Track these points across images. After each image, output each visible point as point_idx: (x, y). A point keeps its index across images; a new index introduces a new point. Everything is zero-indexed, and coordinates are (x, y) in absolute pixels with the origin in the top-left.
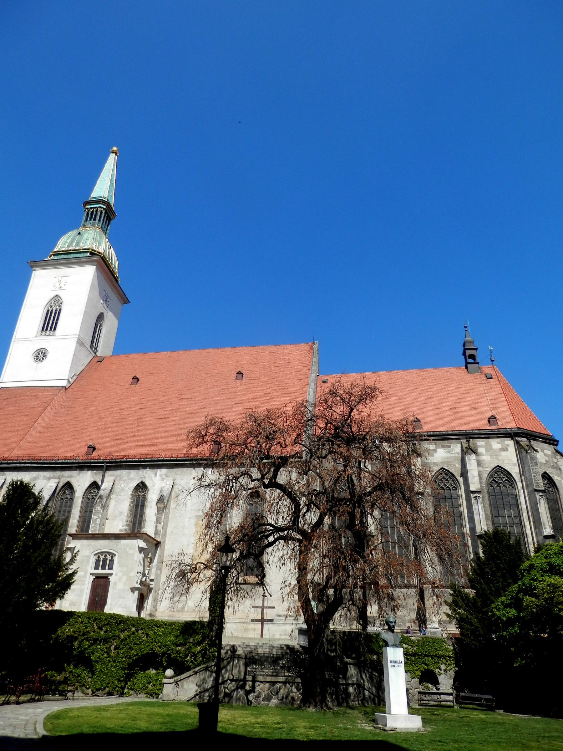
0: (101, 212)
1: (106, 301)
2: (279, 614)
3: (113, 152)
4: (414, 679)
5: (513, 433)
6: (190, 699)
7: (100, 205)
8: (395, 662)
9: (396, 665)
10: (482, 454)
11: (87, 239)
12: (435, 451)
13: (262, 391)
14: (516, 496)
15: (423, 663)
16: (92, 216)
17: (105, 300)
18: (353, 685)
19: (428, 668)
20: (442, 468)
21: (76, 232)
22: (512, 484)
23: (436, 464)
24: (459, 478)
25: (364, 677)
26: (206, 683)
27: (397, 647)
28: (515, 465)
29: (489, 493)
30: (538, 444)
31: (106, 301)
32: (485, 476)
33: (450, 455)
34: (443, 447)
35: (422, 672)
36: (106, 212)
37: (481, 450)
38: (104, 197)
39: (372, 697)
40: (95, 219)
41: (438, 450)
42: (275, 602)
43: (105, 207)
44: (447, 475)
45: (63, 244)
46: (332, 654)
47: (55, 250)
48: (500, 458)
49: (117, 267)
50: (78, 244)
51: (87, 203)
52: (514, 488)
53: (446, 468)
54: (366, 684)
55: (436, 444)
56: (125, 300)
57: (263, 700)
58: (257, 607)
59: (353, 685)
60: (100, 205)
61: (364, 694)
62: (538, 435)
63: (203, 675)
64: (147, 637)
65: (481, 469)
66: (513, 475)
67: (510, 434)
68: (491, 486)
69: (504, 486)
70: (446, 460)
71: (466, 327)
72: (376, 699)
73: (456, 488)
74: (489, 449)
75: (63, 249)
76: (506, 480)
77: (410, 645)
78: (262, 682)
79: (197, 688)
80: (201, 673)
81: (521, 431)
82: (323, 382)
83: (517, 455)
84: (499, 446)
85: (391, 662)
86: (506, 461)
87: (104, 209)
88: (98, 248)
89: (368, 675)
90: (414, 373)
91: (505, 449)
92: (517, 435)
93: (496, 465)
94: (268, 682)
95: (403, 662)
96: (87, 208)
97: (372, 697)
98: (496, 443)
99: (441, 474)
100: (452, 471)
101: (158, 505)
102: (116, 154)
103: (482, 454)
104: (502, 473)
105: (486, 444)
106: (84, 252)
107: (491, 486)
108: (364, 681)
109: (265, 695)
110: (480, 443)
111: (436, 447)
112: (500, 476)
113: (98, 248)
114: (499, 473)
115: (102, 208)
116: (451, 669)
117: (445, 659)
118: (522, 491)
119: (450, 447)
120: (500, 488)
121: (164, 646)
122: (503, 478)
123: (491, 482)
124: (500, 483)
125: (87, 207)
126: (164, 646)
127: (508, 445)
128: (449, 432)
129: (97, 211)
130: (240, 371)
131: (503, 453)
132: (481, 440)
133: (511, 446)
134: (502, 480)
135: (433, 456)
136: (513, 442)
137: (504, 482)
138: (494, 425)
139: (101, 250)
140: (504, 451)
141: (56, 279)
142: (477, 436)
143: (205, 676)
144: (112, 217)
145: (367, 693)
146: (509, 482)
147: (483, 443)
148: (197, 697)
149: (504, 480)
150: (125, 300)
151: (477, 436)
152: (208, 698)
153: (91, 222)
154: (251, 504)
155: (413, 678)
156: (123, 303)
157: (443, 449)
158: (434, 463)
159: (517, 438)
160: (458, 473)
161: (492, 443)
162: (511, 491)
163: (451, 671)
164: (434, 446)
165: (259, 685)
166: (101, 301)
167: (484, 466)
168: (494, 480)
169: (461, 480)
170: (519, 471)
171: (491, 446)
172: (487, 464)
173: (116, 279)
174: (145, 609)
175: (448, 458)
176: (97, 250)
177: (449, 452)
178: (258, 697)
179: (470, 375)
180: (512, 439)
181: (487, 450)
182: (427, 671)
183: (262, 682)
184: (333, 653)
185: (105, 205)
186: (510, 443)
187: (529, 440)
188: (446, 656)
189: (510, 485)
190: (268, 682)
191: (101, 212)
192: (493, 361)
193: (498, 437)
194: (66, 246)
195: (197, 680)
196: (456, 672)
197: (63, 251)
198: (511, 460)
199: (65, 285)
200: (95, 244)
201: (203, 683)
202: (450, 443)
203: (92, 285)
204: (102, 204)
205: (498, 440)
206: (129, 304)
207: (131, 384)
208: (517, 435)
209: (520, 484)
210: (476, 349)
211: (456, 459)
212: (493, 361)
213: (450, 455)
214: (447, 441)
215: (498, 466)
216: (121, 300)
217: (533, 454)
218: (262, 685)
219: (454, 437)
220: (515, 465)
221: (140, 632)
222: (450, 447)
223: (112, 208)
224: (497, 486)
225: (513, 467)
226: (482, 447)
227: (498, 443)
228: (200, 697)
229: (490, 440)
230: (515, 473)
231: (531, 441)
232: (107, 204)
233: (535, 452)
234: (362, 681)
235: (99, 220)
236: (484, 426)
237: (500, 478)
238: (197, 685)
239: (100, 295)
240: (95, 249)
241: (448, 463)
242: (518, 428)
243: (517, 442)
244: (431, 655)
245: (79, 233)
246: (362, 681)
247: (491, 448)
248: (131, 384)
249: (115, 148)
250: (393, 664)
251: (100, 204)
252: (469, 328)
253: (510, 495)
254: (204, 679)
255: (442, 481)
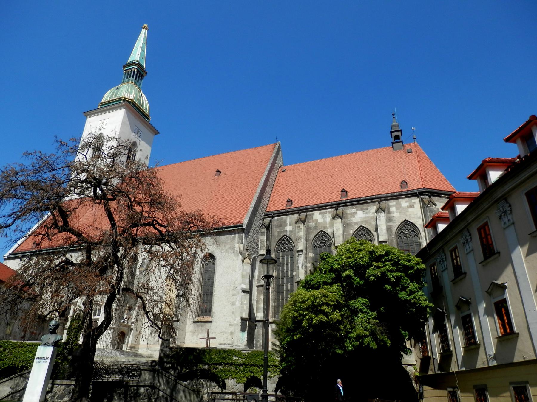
0: (134, 71)
1: (138, 133)
2: (221, 343)
3: (144, 28)
4: (240, 384)
5: (419, 193)
6: (2, 398)
7: (134, 67)
8: (41, 358)
9: (42, 360)
10: (393, 212)
11: (122, 91)
12: (356, 213)
13: (230, 182)
14: (420, 243)
15: (250, 372)
16: (128, 74)
17: (136, 132)
18: (144, 386)
19: (253, 375)
20: (361, 226)
21: (116, 88)
22: (417, 234)
23: (356, 223)
24: (373, 233)
25: (161, 380)
26: (19, 387)
27: (49, 346)
28: (419, 218)
29: (397, 243)
30: (442, 200)
31: (138, 133)
32: (394, 229)
33: (367, 215)
34: (362, 209)
35: (247, 378)
36: (138, 71)
37: (393, 209)
38: (136, 61)
39: (165, 396)
40: (130, 77)
41: (358, 212)
42: (219, 334)
43: (137, 67)
44: (365, 231)
45: (107, 97)
46: (168, 366)
47: (102, 102)
48: (408, 214)
49: (148, 108)
50: (116, 95)
51: (125, 66)
52: (418, 237)
53: (364, 226)
54: (162, 387)
55: (356, 207)
56: (156, 132)
57: (57, 398)
58: (203, 339)
59: (144, 386)
60: (134, 67)
61: (158, 395)
62: (443, 192)
63: (18, 380)
64: (11, 355)
65: (391, 224)
66: (418, 226)
67: (416, 193)
68: (400, 237)
69: (411, 236)
70: (364, 220)
71: (393, 115)
72: (169, 398)
73: (371, 241)
74: (399, 207)
75: (107, 100)
76: (412, 231)
77: (240, 358)
78: (59, 384)
79: (10, 390)
80: (16, 378)
81: (425, 190)
82: (283, 171)
83: (421, 210)
84: (408, 204)
85: (38, 358)
86: (412, 216)
87: (136, 69)
88: (129, 96)
89: (165, 380)
90: (351, 156)
91: (412, 206)
92: (422, 193)
93: (404, 219)
94: (63, 384)
95: (49, 359)
96: (125, 70)
97: (165, 396)
98: (404, 202)
99: (360, 231)
100: (369, 227)
101: (140, 269)
102: (146, 29)
103: (393, 212)
104: (409, 225)
105: (396, 203)
106: (119, 101)
107: (400, 237)
108: (160, 384)
109: (59, 395)
110: (392, 203)
111: (357, 210)
112: (408, 228)
113: (129, 96)
114: (406, 226)
115: (134, 68)
116: (276, 375)
117: (271, 368)
118: (424, 239)
119: (368, 209)
120: (407, 238)
121: (23, 361)
122: (410, 229)
123: (400, 234)
124: (407, 233)
125: (125, 69)
126: (23, 361)
127: (414, 203)
128: (367, 197)
129: (131, 71)
130: (343, 189)
131: (410, 210)
132: (392, 201)
133: (416, 203)
134: (409, 231)
135: (354, 217)
136: (418, 199)
137: (410, 232)
138: (405, 188)
139: (131, 97)
140: (411, 208)
141: (101, 122)
142: (389, 198)
143: (19, 381)
144: (144, 75)
145: (161, 393)
146: (415, 232)
147: (394, 203)
148: (10, 397)
149: (410, 231)
150: (156, 132)
151: (389, 198)
152: (18, 397)
153: (127, 79)
154: (207, 263)
155: (238, 384)
156: (154, 134)
157: (362, 211)
158: (354, 223)
159: (422, 196)
160: (373, 229)
161: (401, 202)
162: (415, 239)
163: (275, 377)
164: (355, 209)
165: (57, 387)
166: (133, 134)
167: (395, 221)
168: (402, 232)
169: (375, 234)
170: (422, 223)
171: (400, 205)
172: (396, 220)
173: (147, 117)
174: (126, 343)
175: (365, 217)
176: (128, 97)
177: (366, 213)
178: (54, 396)
179: (395, 151)
180: (418, 197)
181: (397, 209)
182: (252, 377)
183: (59, 384)
184: (169, 364)
185: (136, 66)
186: (416, 201)
187: (430, 196)
188: (271, 365)
189: (416, 235)
190: (63, 384)
191: (134, 71)
192: (415, 138)
193: (406, 197)
194: (109, 98)
195: (12, 384)
196: (279, 378)
197: (106, 102)
198: (416, 214)
199: (106, 125)
200: (127, 94)
201: (16, 386)
202: (368, 206)
203: (123, 122)
204: (135, 66)
205: (407, 199)
206: (159, 134)
207: (215, 176)
208: (422, 193)
209: (423, 233)
210: (401, 131)
211: (372, 218)
212: (415, 138)
213: (367, 215)
214: (365, 205)
215: (406, 220)
216: (152, 132)
217: (432, 208)
218: (59, 387)
219: (371, 201)
220: (419, 218)
221: (7, 351)
222: (368, 209)
223: (144, 69)
224: (405, 236)
225: (418, 220)
226: (393, 206)
227: (407, 202)
228: (12, 397)
229: (400, 200)
230: (420, 224)
231: (432, 197)
232: (139, 65)
233: (434, 206)
234: (158, 384)
235: (133, 77)
236: (397, 189)
237: (407, 229)
238: (11, 388)
239: (131, 130)
240: (126, 97)
241: (366, 222)
242: (424, 188)
243: (422, 199)
244: (257, 365)
245: (118, 88)
246: (158, 384)
247: (401, 207)
248: (215, 176)
249: (146, 25)
250: (39, 360)
251: (133, 65)
252: (396, 115)
253: (415, 243)
254: (18, 383)
255: (361, 236)
